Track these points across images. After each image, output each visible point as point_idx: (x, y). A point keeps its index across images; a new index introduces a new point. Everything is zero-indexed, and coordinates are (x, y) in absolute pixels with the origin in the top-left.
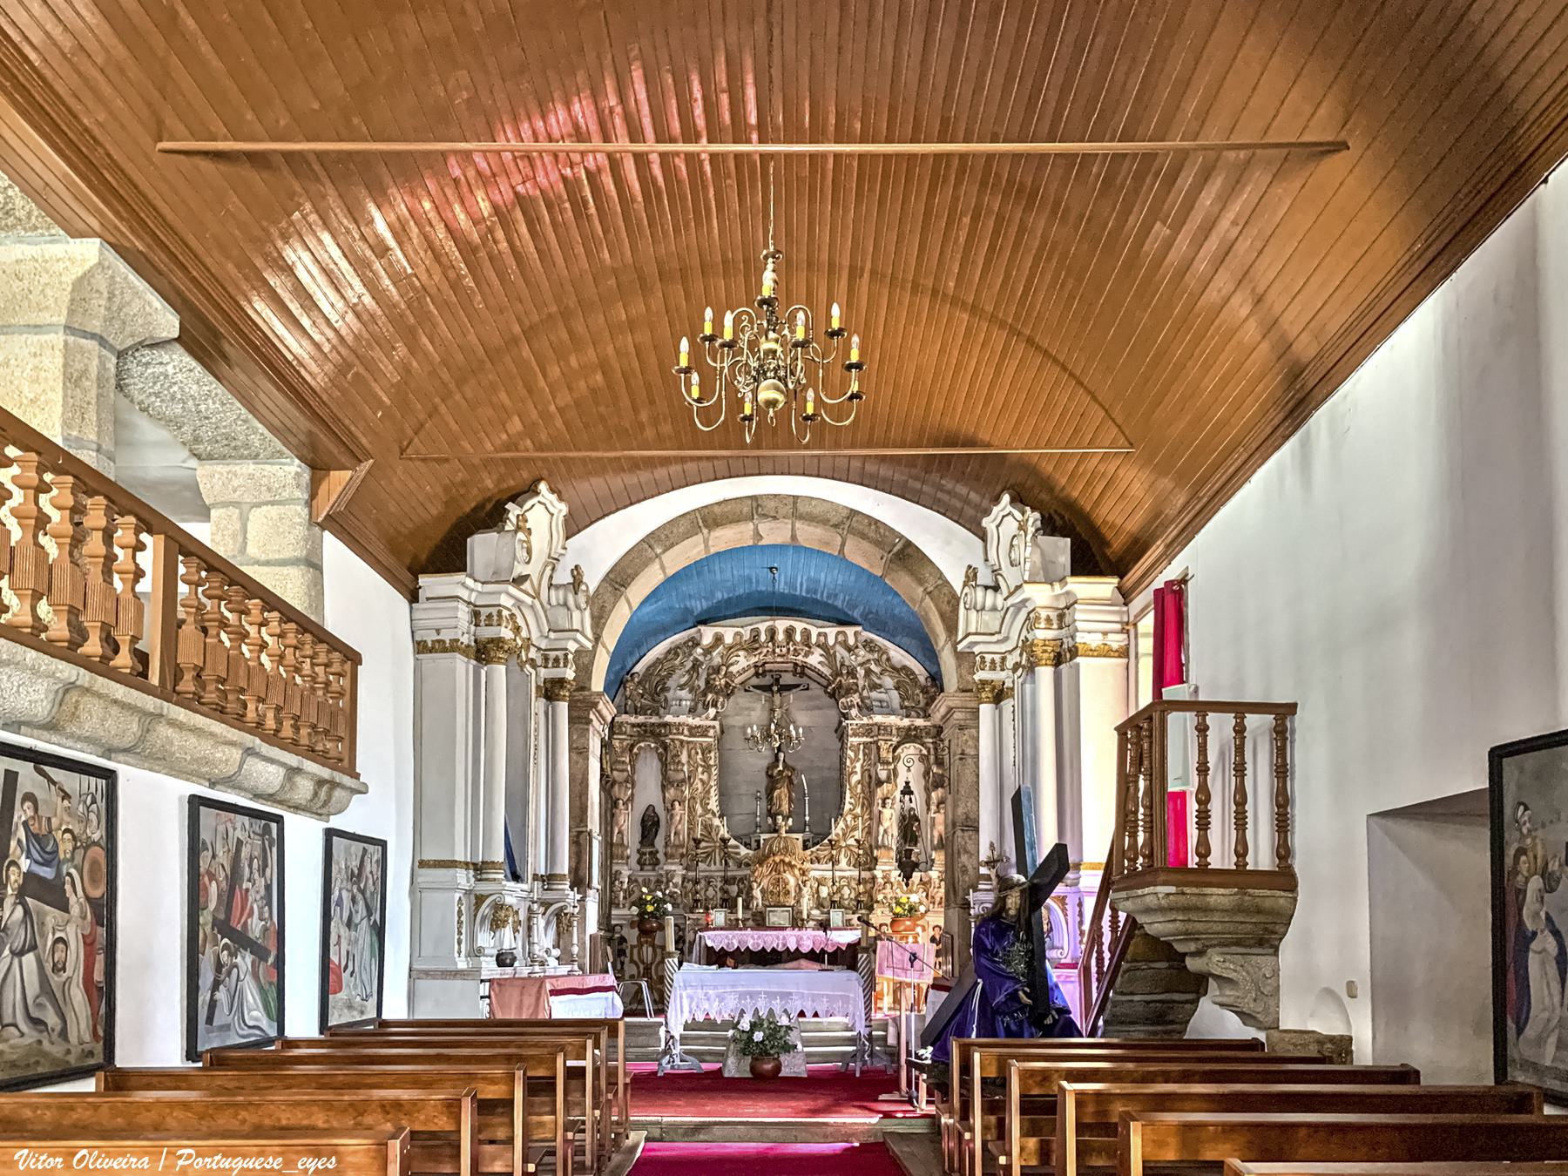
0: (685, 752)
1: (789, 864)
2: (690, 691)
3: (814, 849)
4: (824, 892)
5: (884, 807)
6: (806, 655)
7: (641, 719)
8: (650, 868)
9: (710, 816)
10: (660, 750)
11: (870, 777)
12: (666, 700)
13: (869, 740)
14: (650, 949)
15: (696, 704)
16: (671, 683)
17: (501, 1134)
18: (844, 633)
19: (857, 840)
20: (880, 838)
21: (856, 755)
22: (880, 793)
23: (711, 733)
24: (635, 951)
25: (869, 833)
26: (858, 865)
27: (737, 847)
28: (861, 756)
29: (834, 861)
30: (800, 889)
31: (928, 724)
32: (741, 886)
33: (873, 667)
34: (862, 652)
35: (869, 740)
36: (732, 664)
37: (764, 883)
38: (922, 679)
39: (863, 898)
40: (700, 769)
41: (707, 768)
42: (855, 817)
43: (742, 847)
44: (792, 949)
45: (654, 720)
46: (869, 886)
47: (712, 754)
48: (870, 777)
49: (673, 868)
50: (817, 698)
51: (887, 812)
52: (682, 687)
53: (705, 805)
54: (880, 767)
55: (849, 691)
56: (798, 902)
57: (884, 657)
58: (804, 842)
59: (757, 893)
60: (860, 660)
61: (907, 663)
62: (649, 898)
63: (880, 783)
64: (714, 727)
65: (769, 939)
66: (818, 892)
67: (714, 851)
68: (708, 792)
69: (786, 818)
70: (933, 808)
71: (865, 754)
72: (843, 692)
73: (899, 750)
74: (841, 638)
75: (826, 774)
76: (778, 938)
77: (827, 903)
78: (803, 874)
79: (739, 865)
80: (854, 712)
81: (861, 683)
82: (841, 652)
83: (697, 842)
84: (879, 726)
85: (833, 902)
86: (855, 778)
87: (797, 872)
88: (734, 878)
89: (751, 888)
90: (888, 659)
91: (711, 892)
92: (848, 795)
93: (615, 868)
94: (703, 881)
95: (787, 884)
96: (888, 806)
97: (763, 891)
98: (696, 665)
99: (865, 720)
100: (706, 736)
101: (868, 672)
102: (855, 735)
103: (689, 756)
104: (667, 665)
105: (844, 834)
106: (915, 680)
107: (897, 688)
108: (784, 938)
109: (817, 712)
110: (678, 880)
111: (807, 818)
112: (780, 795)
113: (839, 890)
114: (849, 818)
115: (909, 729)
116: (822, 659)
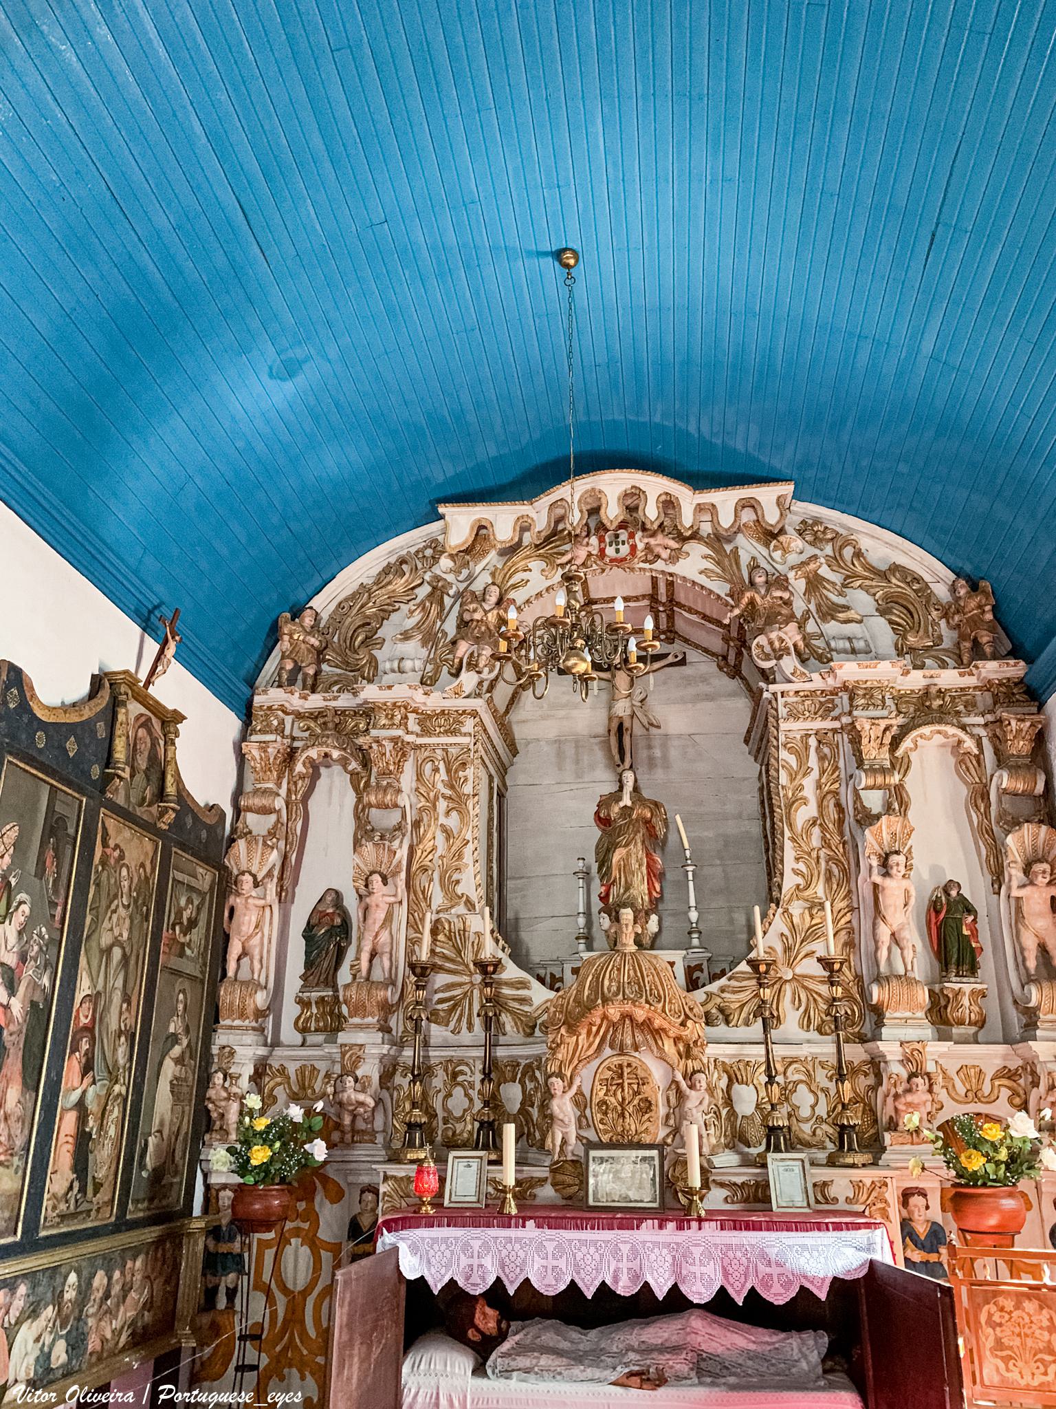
0: (409, 767)
1: (646, 1026)
2: (424, 643)
3: (714, 987)
4: (747, 1100)
5: (887, 874)
6: (674, 558)
7: (316, 701)
8: (320, 1038)
9: (461, 909)
10: (354, 765)
11: (839, 806)
12: (373, 661)
13: (828, 724)
14: (305, 1251)
15: (437, 671)
16: (387, 630)
17: (1006, 798)
18: (751, 504)
19: (826, 963)
20: (883, 954)
21: (802, 757)
22: (872, 841)
23: (469, 725)
24: (269, 1254)
25: (850, 944)
26: (833, 1024)
27: (523, 985)
28: (813, 761)
29: (770, 1021)
30: (681, 1096)
31: (971, 681)
32: (530, 1085)
33: (824, 571)
34: (798, 543)
35: (828, 724)
36: (514, 587)
37: (585, 1078)
38: (941, 591)
39: (854, 1118)
40: (442, 805)
41: (458, 803)
42: (815, 906)
43: (535, 984)
44: (660, 1293)
45: (344, 701)
46: (864, 1082)
47: (470, 772)
48: (839, 806)
49: (360, 1038)
50: (704, 679)
51: (894, 888)
52: (406, 636)
53: (449, 885)
54: (864, 780)
55: (773, 618)
56: (676, 1131)
57: (848, 552)
58: (690, 971)
59: (563, 1107)
60: (793, 559)
61: (902, 560)
62: (261, 1124)
63: (867, 819)
64: (474, 714)
65: (588, 1257)
66: (729, 1101)
67: (467, 995)
68: (459, 855)
69: (641, 916)
70: (1015, 874)
71: (822, 758)
72: (760, 622)
73: (907, 743)
74: (747, 516)
75: (731, 828)
76: (616, 1252)
77: (756, 1132)
78: (687, 1054)
79: (530, 1028)
80: (789, 663)
81: (799, 606)
82: (748, 548)
83: (421, 972)
84: (850, 690)
85: (772, 1131)
86: (805, 813)
87: (669, 1047)
88: (514, 1064)
89: (548, 1095)
90: (858, 554)
91: (458, 1101)
92: (789, 852)
93: (221, 1039)
94: (440, 1072)
95: (643, 1082)
96: (898, 869)
97: (580, 1102)
98: (438, 591)
99: (817, 683)
100: (454, 732)
101: (815, 583)
102: (793, 715)
103: (419, 776)
104: (381, 596)
105: (788, 949)
106: (924, 590)
107: (883, 612)
108: (635, 1253)
109: (709, 705)
110: (370, 1069)
111: (694, 915)
112: (626, 860)
113: (787, 1093)
114: (797, 909)
115: (926, 694)
116: (709, 565)
